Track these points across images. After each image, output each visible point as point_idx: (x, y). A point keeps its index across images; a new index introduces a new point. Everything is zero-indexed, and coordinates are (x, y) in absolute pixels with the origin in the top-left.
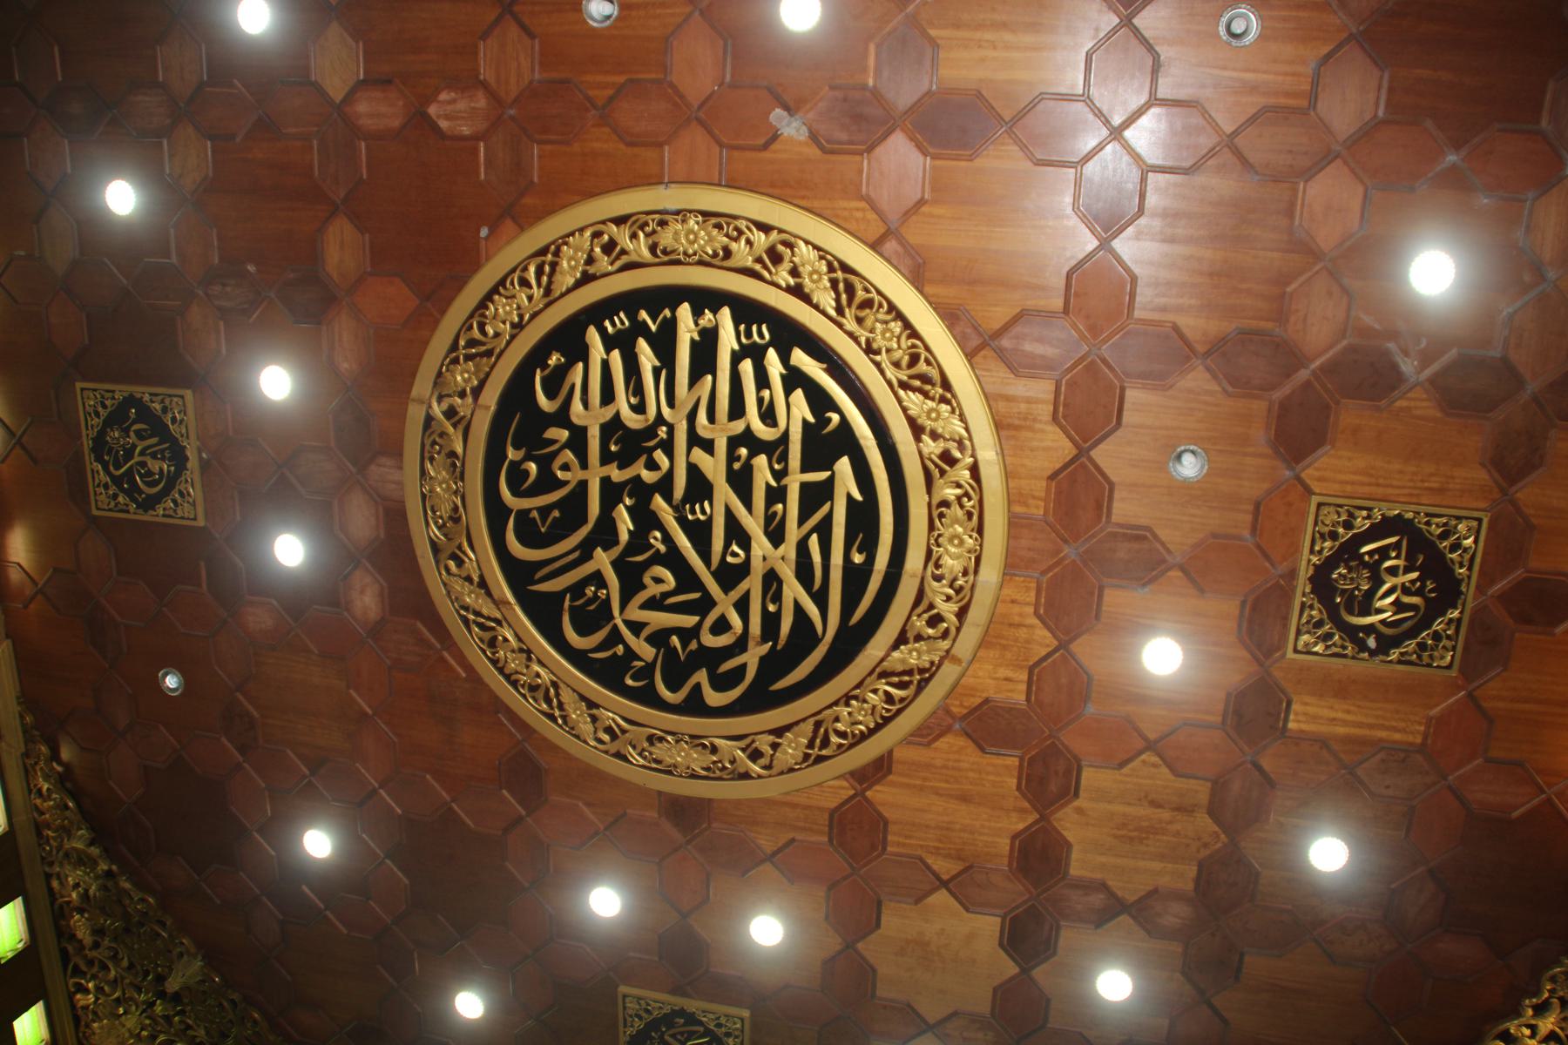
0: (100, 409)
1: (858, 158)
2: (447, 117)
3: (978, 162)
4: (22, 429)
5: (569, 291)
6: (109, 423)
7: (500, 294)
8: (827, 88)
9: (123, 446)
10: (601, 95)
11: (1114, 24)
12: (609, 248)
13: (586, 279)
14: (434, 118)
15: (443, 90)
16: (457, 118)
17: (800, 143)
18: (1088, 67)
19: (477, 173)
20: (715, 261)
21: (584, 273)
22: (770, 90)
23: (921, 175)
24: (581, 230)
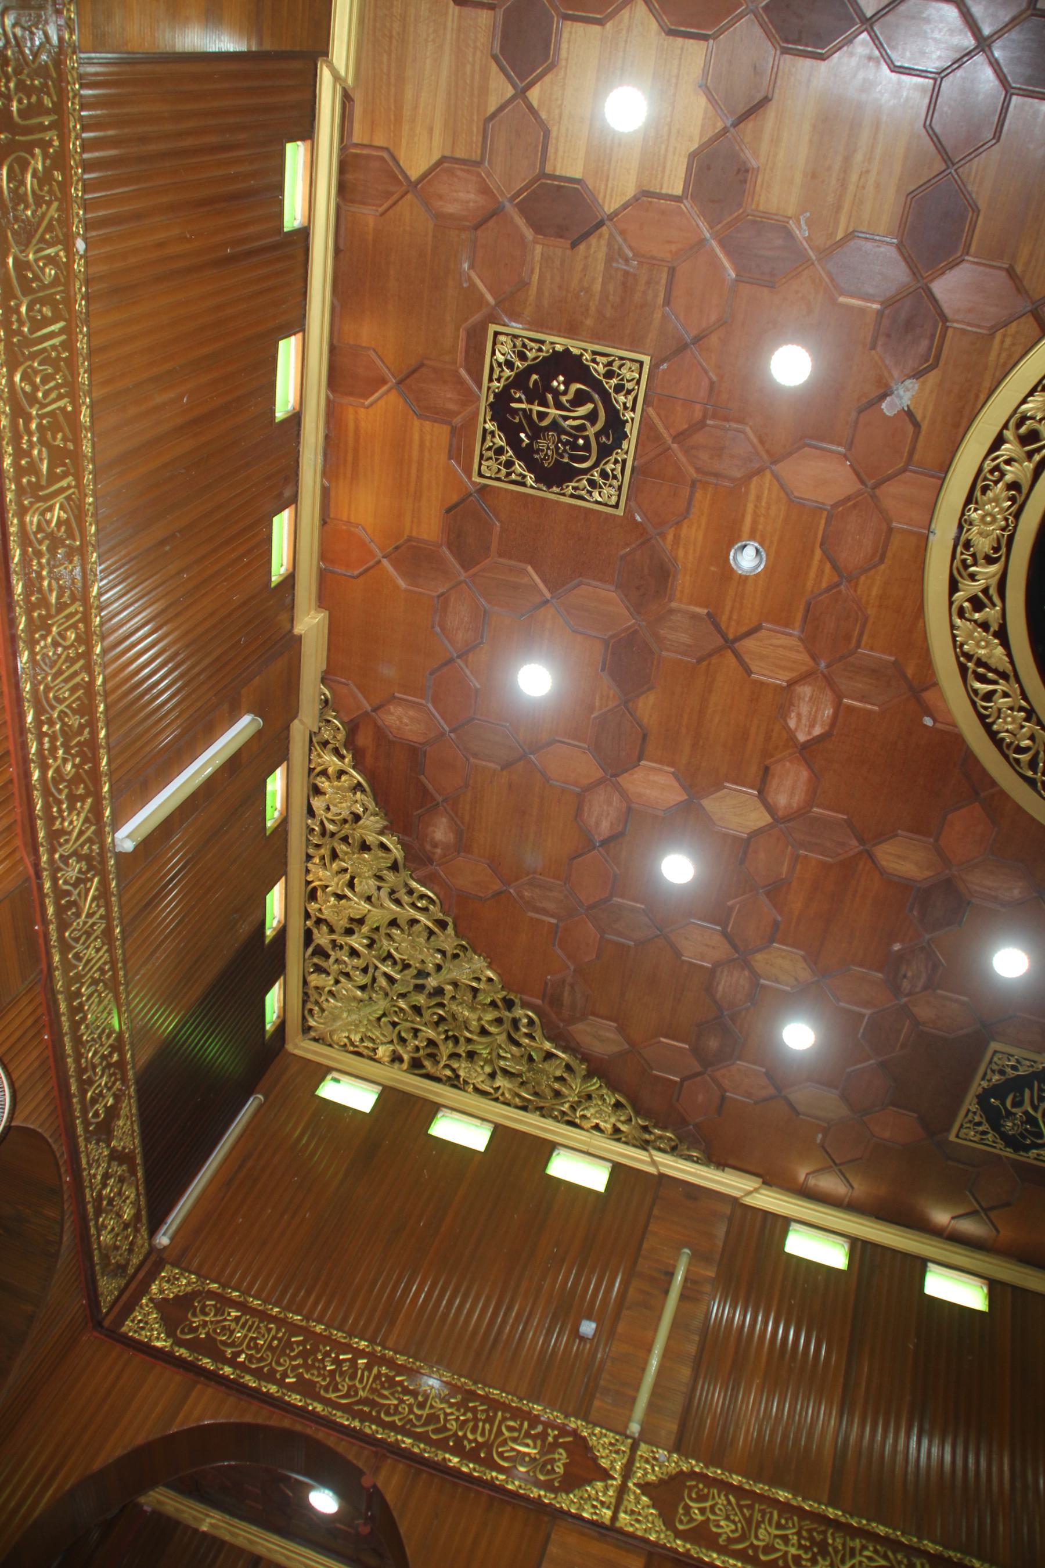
0: (981, 1129)
1: (950, 333)
2: (812, 726)
3: (982, 205)
4: (973, 1200)
5: (1009, 655)
6: (996, 1127)
7: (994, 723)
8: (873, 352)
9: (1022, 1123)
10: (828, 576)
11: (868, 38)
12: (977, 604)
13: (1002, 635)
14: (809, 738)
15: (787, 724)
16: (815, 717)
17: (921, 390)
18: (907, 71)
19: (870, 712)
20: (1020, 501)
21: (996, 635)
22: (861, 411)
23: (982, 268)
24: (953, 627)
